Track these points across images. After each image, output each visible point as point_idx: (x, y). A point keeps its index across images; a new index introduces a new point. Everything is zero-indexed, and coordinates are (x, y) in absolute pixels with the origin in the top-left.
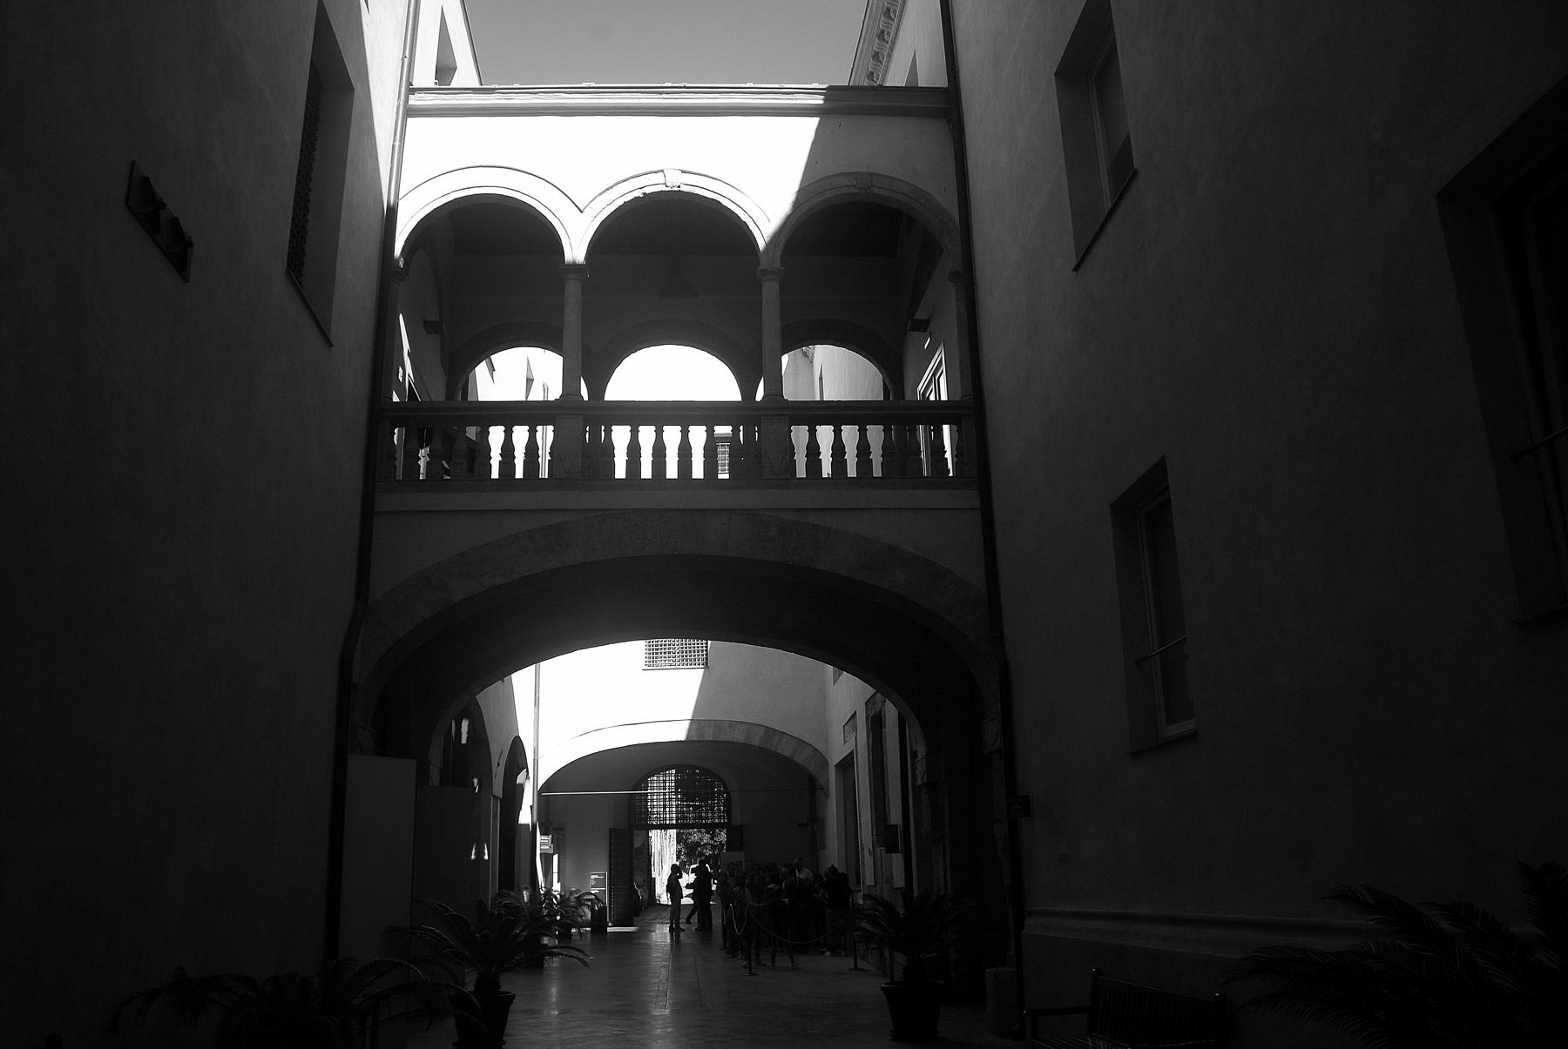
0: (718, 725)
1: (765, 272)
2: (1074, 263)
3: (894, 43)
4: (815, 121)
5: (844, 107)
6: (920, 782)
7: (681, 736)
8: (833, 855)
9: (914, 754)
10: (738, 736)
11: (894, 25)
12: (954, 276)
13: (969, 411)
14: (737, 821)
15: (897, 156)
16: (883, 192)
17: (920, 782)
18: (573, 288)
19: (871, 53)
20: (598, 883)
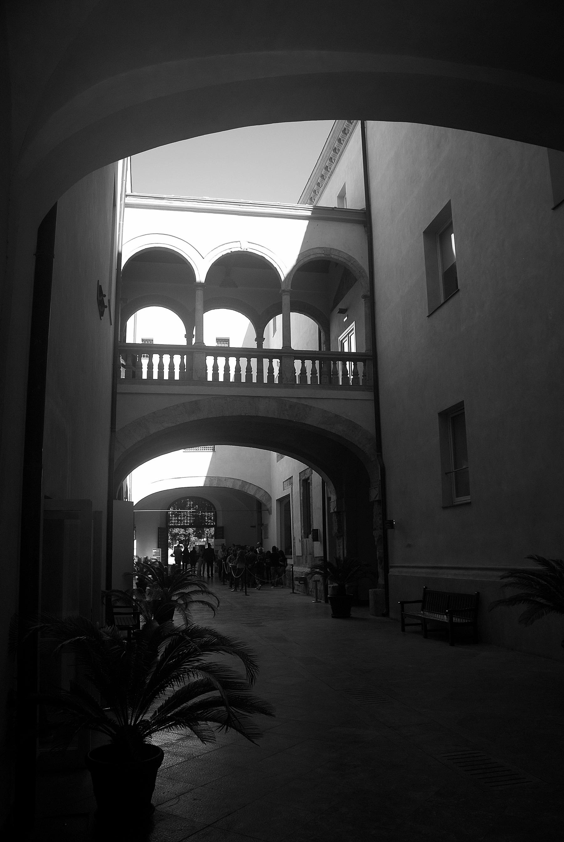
0: (219, 479)
1: (284, 291)
2: (428, 315)
3: (332, 172)
4: (307, 222)
5: (321, 216)
6: (332, 511)
7: (201, 484)
8: (273, 539)
9: (329, 499)
10: (229, 485)
11: (334, 165)
12: (365, 297)
13: (369, 357)
14: (220, 524)
15: (342, 241)
16: (335, 257)
17: (332, 511)
18: (199, 294)
19: (320, 175)
20: (156, 554)
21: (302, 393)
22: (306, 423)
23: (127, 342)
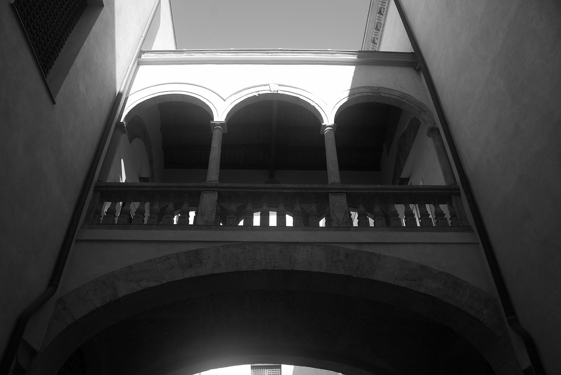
4: (353, 68)
5: (370, 59)
12: (433, 131)
15: (397, 82)
16: (386, 95)
21: (363, 237)
22: (374, 278)
23: (270, 225)
